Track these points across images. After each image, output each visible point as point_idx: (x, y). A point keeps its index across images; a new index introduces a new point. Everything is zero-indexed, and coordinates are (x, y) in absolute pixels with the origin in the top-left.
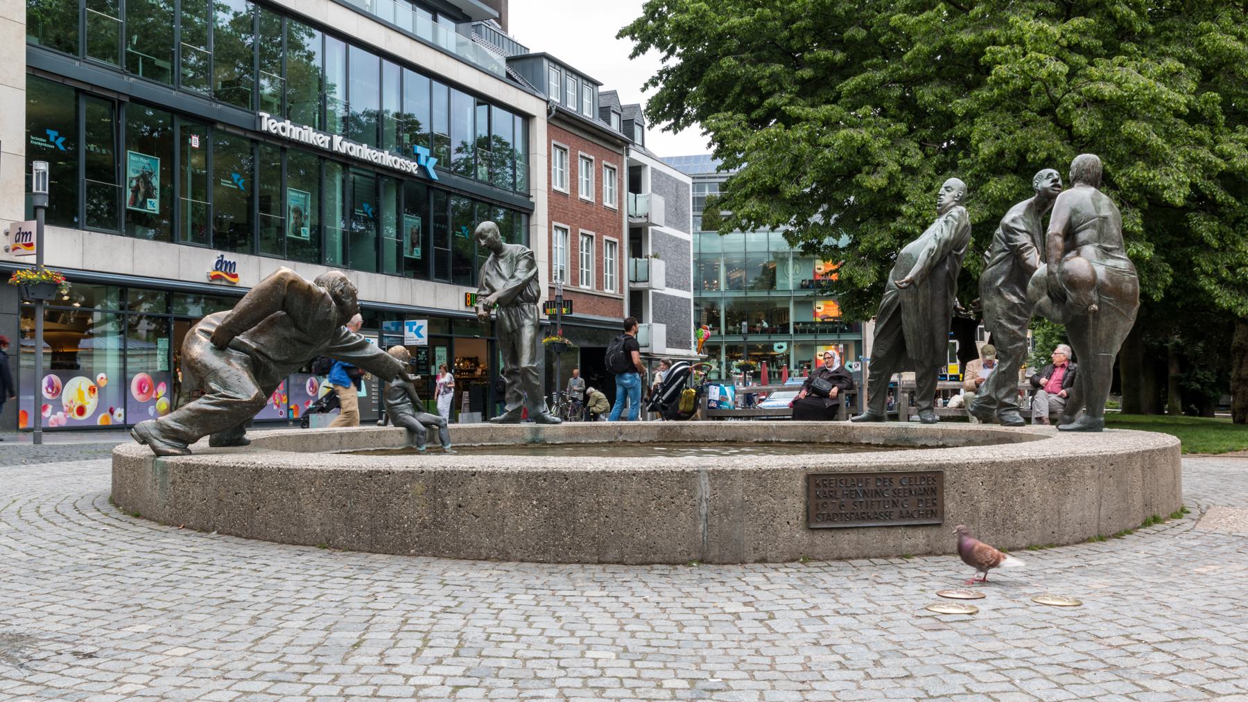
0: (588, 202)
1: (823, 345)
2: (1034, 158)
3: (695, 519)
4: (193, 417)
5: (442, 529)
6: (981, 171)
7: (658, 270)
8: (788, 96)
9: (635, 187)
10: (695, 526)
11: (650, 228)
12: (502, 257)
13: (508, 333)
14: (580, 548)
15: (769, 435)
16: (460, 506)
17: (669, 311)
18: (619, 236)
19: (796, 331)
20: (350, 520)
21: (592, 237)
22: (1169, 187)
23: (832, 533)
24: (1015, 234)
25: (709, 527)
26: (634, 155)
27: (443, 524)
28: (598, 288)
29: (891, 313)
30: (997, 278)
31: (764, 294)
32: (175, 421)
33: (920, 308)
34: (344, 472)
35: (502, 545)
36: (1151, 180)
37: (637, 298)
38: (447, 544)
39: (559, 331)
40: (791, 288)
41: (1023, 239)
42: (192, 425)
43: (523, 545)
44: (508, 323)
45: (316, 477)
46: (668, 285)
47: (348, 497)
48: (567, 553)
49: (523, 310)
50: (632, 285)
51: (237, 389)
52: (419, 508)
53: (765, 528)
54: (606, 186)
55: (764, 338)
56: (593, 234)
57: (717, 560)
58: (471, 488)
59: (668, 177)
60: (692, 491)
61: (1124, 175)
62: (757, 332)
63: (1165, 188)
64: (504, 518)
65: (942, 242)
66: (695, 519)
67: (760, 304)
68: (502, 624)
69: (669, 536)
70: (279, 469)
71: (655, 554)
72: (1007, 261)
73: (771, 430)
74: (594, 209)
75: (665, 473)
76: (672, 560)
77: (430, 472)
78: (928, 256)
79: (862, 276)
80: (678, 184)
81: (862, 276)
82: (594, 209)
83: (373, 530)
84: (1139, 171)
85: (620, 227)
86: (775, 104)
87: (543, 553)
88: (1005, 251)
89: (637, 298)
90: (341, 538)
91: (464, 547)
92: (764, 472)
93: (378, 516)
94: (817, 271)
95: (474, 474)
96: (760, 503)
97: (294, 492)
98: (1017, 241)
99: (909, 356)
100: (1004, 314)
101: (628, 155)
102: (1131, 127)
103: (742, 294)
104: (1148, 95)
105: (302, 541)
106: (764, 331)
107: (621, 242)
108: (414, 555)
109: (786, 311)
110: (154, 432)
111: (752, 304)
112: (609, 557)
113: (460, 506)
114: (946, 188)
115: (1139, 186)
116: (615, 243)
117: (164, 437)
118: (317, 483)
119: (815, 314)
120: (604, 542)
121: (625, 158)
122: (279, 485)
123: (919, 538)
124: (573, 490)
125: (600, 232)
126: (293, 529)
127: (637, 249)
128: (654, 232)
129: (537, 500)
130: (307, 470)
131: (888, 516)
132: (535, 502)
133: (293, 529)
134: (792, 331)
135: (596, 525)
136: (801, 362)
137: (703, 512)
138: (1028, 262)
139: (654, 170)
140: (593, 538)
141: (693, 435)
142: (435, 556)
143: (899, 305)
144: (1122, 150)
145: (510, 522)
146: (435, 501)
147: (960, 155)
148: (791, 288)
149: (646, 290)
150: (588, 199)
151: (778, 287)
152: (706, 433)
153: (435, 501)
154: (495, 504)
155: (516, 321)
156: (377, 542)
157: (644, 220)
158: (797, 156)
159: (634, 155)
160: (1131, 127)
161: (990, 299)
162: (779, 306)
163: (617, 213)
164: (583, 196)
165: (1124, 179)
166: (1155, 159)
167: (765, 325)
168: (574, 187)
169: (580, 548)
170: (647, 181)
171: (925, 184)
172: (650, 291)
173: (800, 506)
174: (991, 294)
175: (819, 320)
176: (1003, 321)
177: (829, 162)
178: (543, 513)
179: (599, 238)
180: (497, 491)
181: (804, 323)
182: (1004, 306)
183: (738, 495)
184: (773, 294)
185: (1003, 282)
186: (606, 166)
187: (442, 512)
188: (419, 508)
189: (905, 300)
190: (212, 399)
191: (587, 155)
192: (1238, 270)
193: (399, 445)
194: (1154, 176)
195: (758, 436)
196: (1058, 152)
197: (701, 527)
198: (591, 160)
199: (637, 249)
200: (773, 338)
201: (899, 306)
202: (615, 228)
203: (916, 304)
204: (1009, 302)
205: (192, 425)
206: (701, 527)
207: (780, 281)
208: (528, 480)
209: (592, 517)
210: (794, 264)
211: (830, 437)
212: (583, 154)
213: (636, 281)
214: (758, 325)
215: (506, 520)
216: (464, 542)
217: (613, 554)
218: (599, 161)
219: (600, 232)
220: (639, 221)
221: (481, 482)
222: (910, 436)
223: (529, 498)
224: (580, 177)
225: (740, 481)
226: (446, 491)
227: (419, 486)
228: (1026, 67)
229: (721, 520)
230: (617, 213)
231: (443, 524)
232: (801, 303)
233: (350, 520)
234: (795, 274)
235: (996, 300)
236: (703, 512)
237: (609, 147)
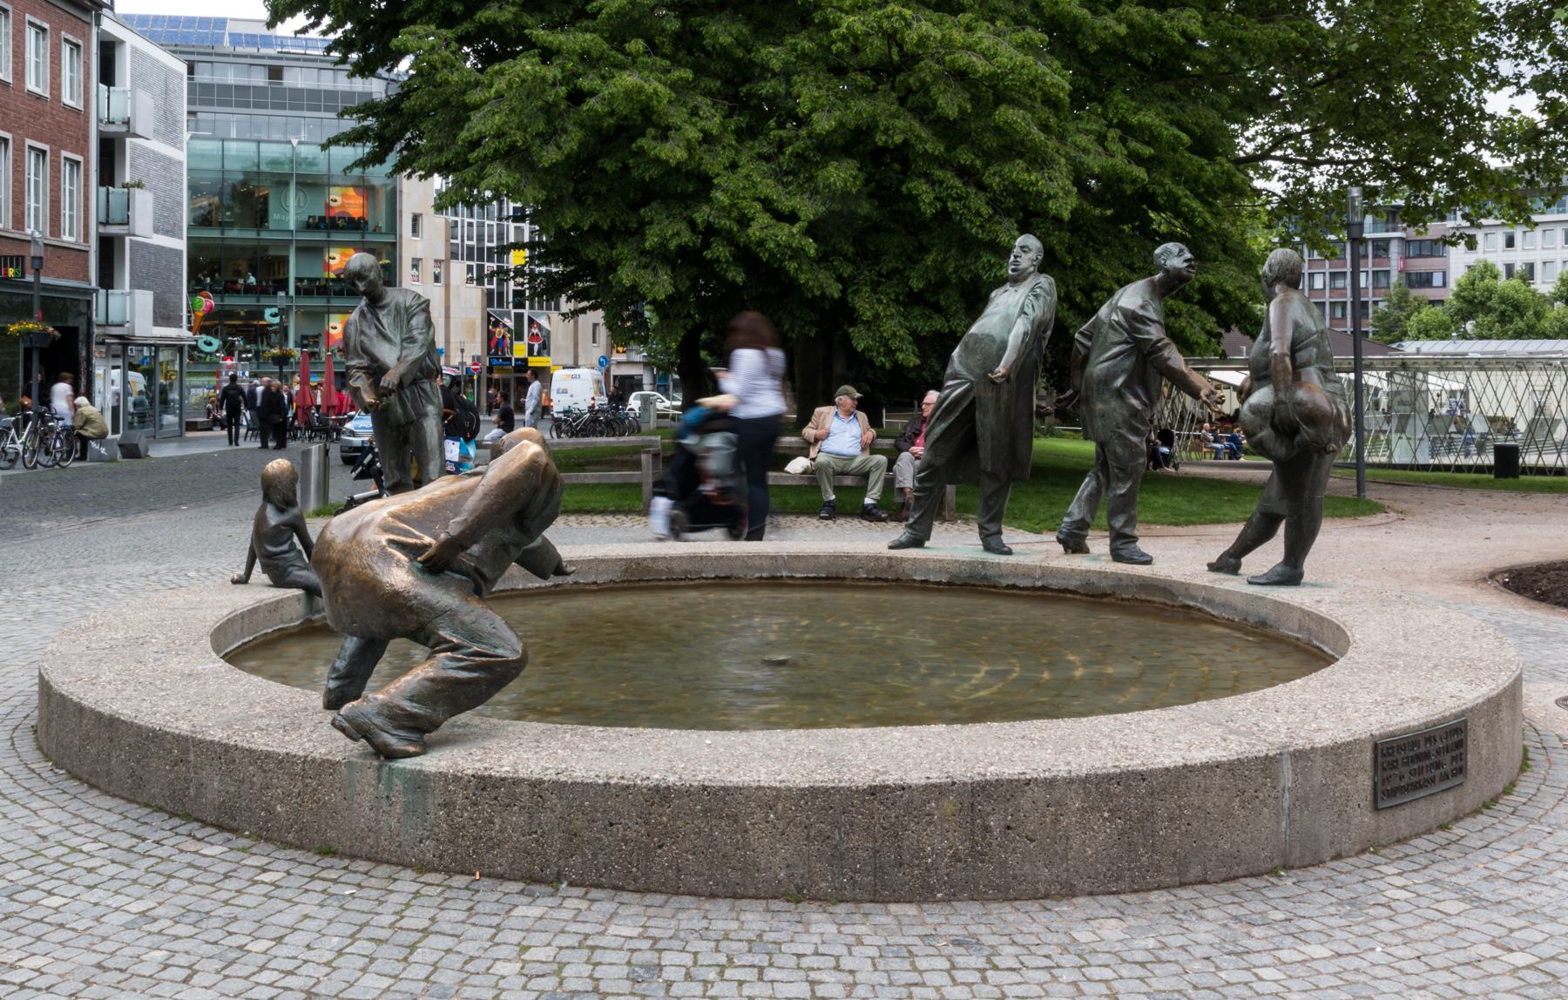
0: (39, 97)
1: (339, 312)
2: (886, 142)
3: (1277, 815)
4: (437, 691)
5: (982, 862)
6: (807, 148)
7: (144, 206)
8: (511, 9)
9: (107, 76)
10: (1278, 823)
11: (128, 140)
12: (383, 307)
13: (399, 426)
14: (1159, 869)
15: (778, 569)
16: (1009, 828)
17: (152, 269)
18: (84, 151)
19: (298, 290)
20: (838, 857)
21: (44, 152)
22: (1055, 196)
23: (1392, 812)
24: (1144, 323)
25: (1291, 822)
26: (107, 25)
27: (986, 854)
28: (52, 234)
29: (960, 409)
30: (1116, 377)
31: (251, 234)
32: (411, 699)
33: (1003, 406)
34: (827, 790)
35: (1065, 876)
36: (1033, 184)
37: (109, 248)
38: (990, 881)
39: (37, 314)
40: (292, 227)
41: (1154, 333)
42: (435, 703)
43: (1092, 873)
44: (400, 411)
45: (777, 798)
46: (156, 230)
47: (835, 824)
48: (1144, 878)
49: (424, 390)
50: (102, 230)
51: (494, 641)
52: (950, 835)
53: (1340, 816)
54: (66, 73)
55: (250, 301)
56: (46, 147)
57: (1298, 864)
58: (1024, 803)
59: (155, 61)
60: (1275, 779)
61: (994, 174)
62: (238, 292)
63: (1050, 197)
64: (1068, 839)
65: (1036, 323)
66: (1277, 815)
67: (243, 248)
68: (746, 926)
69: (1253, 840)
70: (705, 788)
71: (1238, 865)
72: (1129, 355)
73: (780, 562)
74: (47, 109)
75: (1249, 760)
76: (1256, 871)
77: (965, 784)
78: (1023, 341)
79: (652, 284)
80: (169, 72)
81: (652, 284)
82: (47, 109)
83: (878, 870)
84: (1017, 171)
85: (86, 138)
86: (495, 20)
87: (1117, 880)
88: (1127, 343)
89: (109, 248)
90: (823, 884)
91: (1015, 883)
92: (1340, 746)
93: (886, 850)
94: (332, 204)
95: (1028, 782)
96: (1336, 786)
97: (736, 821)
98: (1148, 333)
99: (982, 466)
100: (1125, 422)
101: (98, 24)
102: (1007, 114)
103: (214, 233)
104: (1028, 75)
105: (752, 891)
106: (248, 290)
107: (87, 162)
108: (942, 900)
109: (284, 261)
110: (378, 721)
111: (230, 248)
112: (1191, 877)
113: (1009, 828)
114: (1022, 247)
115: (1016, 191)
116: (78, 163)
117: (396, 728)
118: (780, 806)
119: (328, 267)
120: (1185, 857)
121: (94, 30)
122: (705, 811)
123: (1447, 804)
124: (1152, 794)
125: (57, 144)
126: (734, 876)
127: (108, 175)
128: (135, 147)
129: (1110, 811)
130: (759, 788)
131: (1432, 781)
132: (1106, 815)
133: (734, 876)
134: (292, 291)
135: (1177, 837)
136: (304, 337)
137: (1286, 805)
138: (1170, 363)
139: (135, 50)
140: (1174, 855)
141: (670, 571)
142: (973, 899)
143: (974, 399)
144: (991, 141)
145: (1075, 844)
146: (973, 824)
147: (772, 123)
148: (292, 227)
149: (121, 238)
150: (38, 91)
151: (272, 225)
152: (689, 567)
153: (973, 824)
154: (1056, 821)
155: (414, 408)
156: (885, 886)
157: (124, 129)
158: (551, 106)
159: (107, 25)
160: (1007, 114)
161: (1105, 402)
162: (272, 253)
163: (81, 116)
164: (31, 85)
165: (997, 179)
166: (1038, 160)
167: (252, 280)
168: (19, 73)
169: (1159, 869)
170: (125, 66)
171: (728, 158)
172: (127, 239)
173: (1368, 783)
174: (1107, 396)
175: (332, 276)
176: (1123, 431)
177: (599, 117)
178: (1116, 828)
179: (56, 154)
180: (1059, 804)
181: (311, 280)
182: (1126, 413)
183: (1318, 778)
184: (265, 235)
185: (1124, 382)
186: (31, 24)
187: (984, 838)
188: (950, 835)
189: (983, 395)
190: (461, 660)
191: (38, 22)
192: (1095, 295)
193: (297, 619)
194: (1037, 181)
195: (761, 569)
196: (918, 137)
197: (1284, 824)
198: (44, 30)
199: (108, 175)
200: (264, 301)
201: (973, 402)
202: (78, 140)
203: (998, 400)
204: (1133, 406)
205: (435, 703)
206: (1284, 824)
207: (274, 217)
208: (1097, 785)
209: (1173, 827)
210: (297, 190)
211: (868, 572)
212: (33, 19)
213: (106, 223)
214: (241, 281)
215: (1071, 842)
216: (1015, 877)
217: (1195, 872)
218: (56, 32)
219: (57, 144)
220: (112, 129)
221: (1037, 792)
222: (990, 572)
223: (1099, 810)
224: (27, 55)
225: (1319, 762)
226: (989, 809)
227: (949, 805)
228: (886, 24)
229: (1302, 811)
230: (81, 116)
231: (986, 854)
232: (308, 250)
233: (838, 857)
234: (298, 206)
235: (1114, 403)
236: (1286, 805)
237: (72, 11)
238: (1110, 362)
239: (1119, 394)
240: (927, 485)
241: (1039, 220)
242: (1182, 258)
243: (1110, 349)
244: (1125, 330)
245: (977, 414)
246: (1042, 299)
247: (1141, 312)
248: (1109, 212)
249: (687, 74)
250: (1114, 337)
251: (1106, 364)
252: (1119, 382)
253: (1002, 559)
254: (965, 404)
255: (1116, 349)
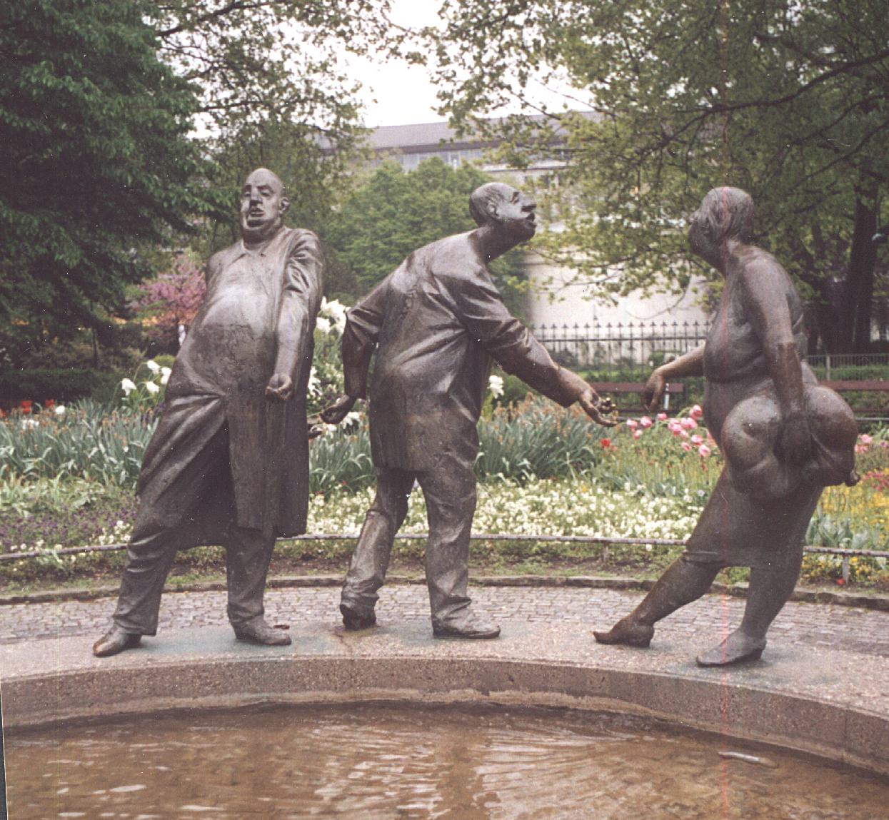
30: (439, 376)
72: (455, 347)
182: (456, 429)
203: (263, 423)
238: (432, 355)
239: (445, 400)
240: (152, 556)
241: (446, 35)
242: (519, 205)
243: (427, 336)
244: (451, 308)
245: (232, 446)
246: (313, 266)
247: (478, 282)
248: (658, 23)
249: (511, 403)
250: (432, 319)
251: (424, 359)
252: (445, 384)
253: (271, 654)
254: (212, 432)
255: (440, 336)
